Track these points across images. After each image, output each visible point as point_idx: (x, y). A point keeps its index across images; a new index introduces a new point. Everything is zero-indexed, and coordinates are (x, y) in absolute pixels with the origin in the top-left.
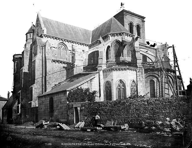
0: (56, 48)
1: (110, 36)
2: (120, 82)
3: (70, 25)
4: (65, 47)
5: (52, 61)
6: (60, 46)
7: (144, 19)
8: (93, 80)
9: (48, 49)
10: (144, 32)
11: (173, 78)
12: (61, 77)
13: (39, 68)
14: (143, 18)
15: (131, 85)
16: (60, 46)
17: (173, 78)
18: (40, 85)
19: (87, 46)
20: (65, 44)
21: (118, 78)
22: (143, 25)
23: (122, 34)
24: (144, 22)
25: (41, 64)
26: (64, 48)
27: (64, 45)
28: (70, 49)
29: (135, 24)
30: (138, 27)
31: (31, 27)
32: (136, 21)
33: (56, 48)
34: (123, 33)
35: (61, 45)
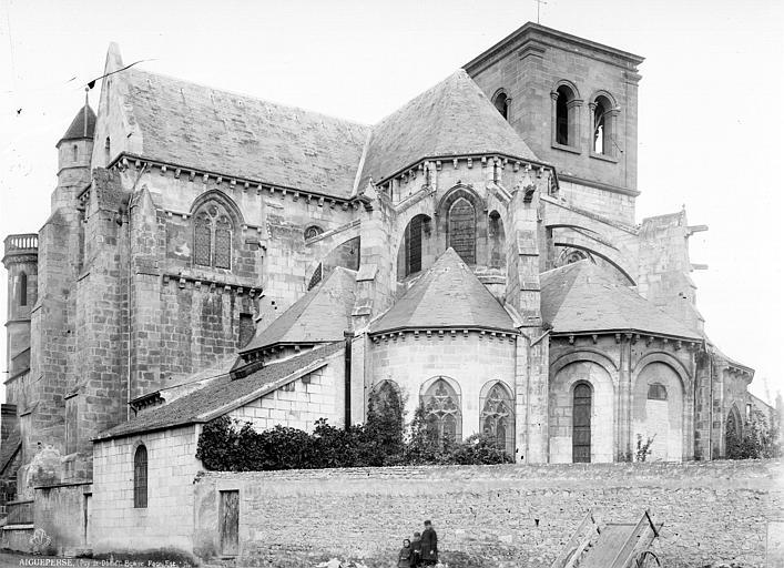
0: (185, 217)
1: (432, 166)
2: (441, 387)
3: (262, 104)
4: (229, 211)
5: (166, 279)
6: (205, 208)
7: (638, 67)
8: (315, 379)
9: (147, 227)
10: (630, 132)
11: (684, 376)
12: (210, 349)
13: (106, 312)
14: (625, 62)
15: (483, 401)
16: (205, 208)
17: (684, 376)
18: (111, 387)
19: (337, 203)
20: (228, 199)
21: (430, 371)
22: (630, 98)
23: (487, 159)
24: (639, 78)
25: (489, 70)
26: (222, 217)
27: (223, 204)
28: (252, 224)
29: (586, 93)
30: (602, 108)
31: (79, 110)
32: (591, 80)
33: (185, 217)
34: (489, 156)
35: (213, 202)
